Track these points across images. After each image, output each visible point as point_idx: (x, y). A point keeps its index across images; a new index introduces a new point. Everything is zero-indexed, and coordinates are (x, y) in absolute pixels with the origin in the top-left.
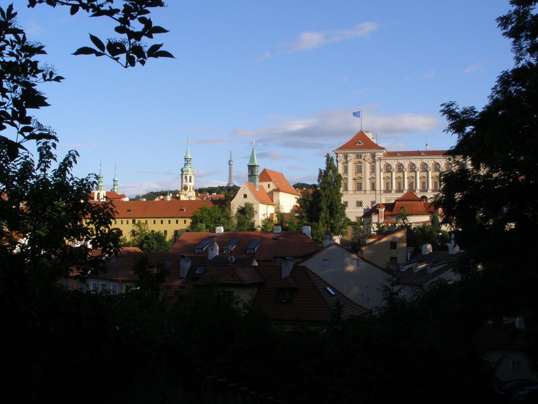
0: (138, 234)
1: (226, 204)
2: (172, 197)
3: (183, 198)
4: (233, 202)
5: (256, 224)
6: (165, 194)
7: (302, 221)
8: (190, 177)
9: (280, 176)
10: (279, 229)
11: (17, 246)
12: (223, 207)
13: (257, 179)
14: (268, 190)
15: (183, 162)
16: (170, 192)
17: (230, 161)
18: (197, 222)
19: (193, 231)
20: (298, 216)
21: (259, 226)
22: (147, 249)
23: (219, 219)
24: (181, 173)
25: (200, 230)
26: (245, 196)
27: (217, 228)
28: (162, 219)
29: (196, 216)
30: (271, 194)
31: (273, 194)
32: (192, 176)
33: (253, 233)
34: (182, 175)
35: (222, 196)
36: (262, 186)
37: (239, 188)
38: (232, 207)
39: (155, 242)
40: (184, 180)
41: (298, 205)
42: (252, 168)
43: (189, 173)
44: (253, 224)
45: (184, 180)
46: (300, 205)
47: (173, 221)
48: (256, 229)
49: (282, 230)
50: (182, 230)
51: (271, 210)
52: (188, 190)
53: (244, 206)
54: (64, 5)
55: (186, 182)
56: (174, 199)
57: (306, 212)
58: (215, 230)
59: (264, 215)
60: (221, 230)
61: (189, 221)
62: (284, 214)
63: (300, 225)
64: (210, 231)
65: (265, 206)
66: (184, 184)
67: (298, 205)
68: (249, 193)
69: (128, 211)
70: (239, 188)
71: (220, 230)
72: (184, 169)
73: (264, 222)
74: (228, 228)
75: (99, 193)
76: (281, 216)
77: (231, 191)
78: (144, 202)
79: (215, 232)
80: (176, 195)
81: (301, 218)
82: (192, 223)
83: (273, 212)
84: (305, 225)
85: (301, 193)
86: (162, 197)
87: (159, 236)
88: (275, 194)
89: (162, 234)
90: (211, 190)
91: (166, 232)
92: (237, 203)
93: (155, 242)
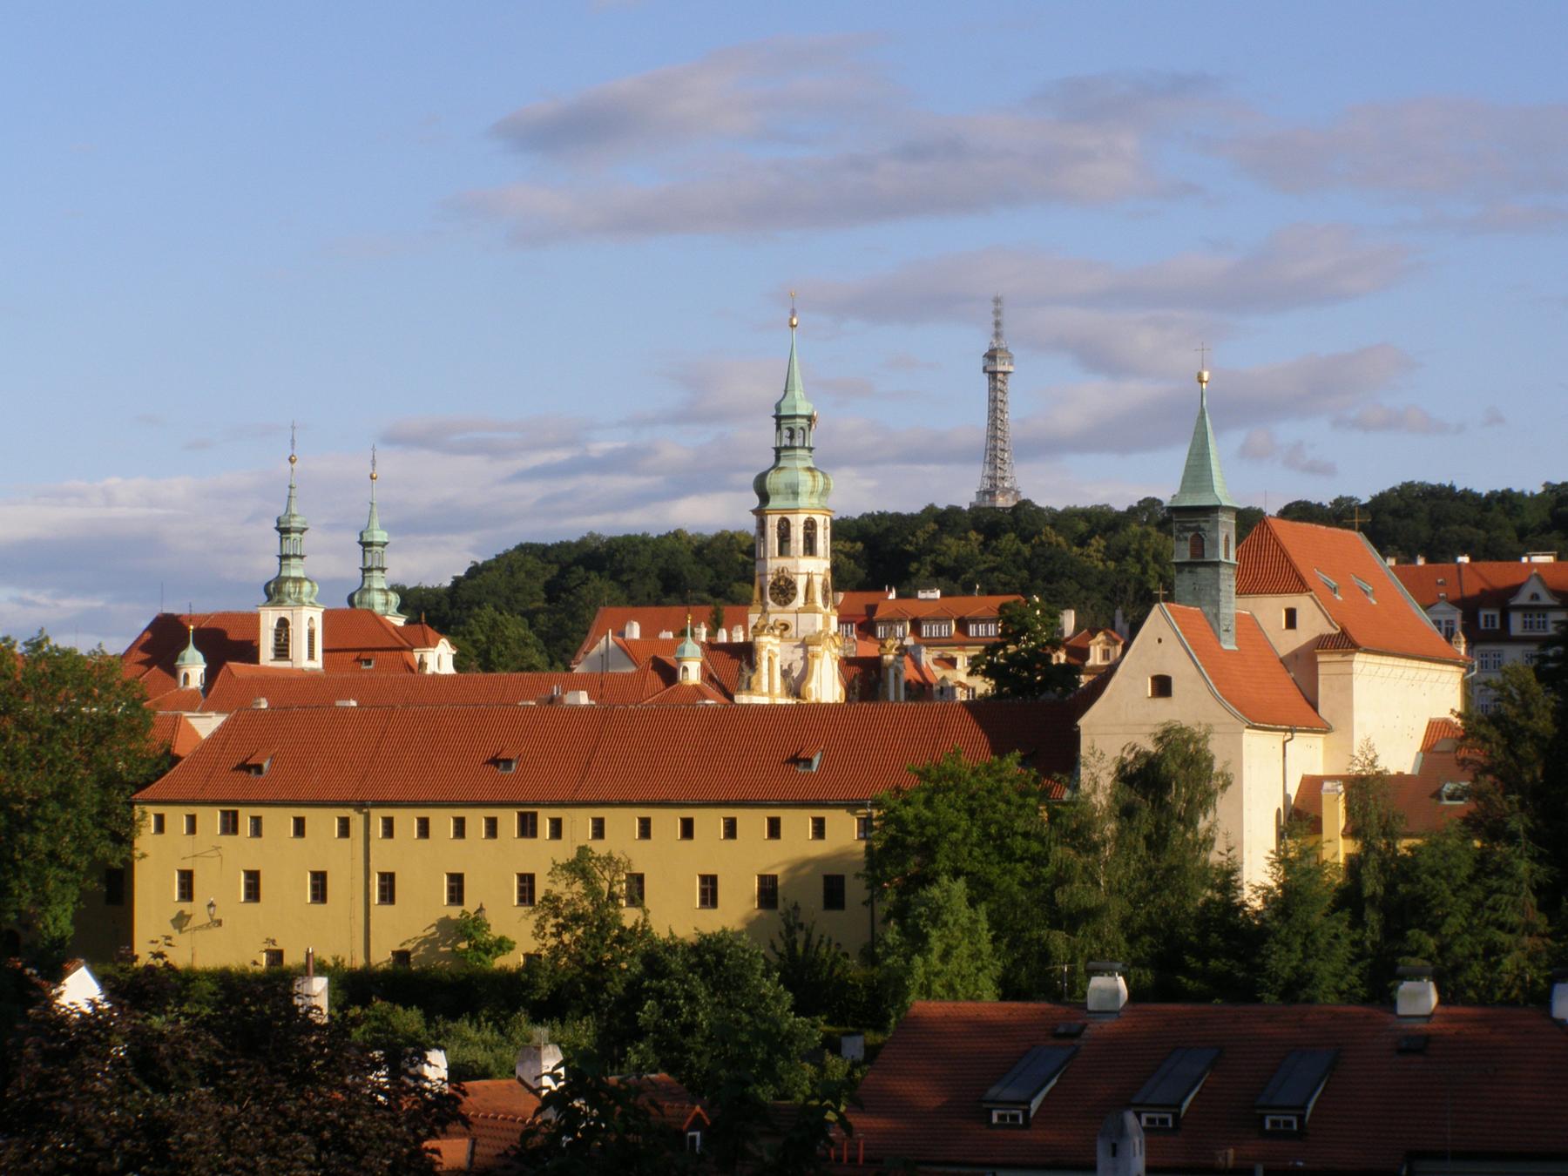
0: (576, 918)
4: (1088, 723)
8: (810, 526)
14: (1288, 643)
15: (768, 435)
17: (991, 356)
22: (658, 1029)
24: (755, 501)
26: (1162, 686)
30: (1303, 665)
36: (1252, 618)
39: (702, 992)
43: (803, 501)
47: (753, 821)
53: (1150, 747)
55: (783, 551)
65: (1273, 740)
69: (495, 761)
75: (283, 624)
78: (577, 709)
88: (1328, 665)
93: (702, 992)
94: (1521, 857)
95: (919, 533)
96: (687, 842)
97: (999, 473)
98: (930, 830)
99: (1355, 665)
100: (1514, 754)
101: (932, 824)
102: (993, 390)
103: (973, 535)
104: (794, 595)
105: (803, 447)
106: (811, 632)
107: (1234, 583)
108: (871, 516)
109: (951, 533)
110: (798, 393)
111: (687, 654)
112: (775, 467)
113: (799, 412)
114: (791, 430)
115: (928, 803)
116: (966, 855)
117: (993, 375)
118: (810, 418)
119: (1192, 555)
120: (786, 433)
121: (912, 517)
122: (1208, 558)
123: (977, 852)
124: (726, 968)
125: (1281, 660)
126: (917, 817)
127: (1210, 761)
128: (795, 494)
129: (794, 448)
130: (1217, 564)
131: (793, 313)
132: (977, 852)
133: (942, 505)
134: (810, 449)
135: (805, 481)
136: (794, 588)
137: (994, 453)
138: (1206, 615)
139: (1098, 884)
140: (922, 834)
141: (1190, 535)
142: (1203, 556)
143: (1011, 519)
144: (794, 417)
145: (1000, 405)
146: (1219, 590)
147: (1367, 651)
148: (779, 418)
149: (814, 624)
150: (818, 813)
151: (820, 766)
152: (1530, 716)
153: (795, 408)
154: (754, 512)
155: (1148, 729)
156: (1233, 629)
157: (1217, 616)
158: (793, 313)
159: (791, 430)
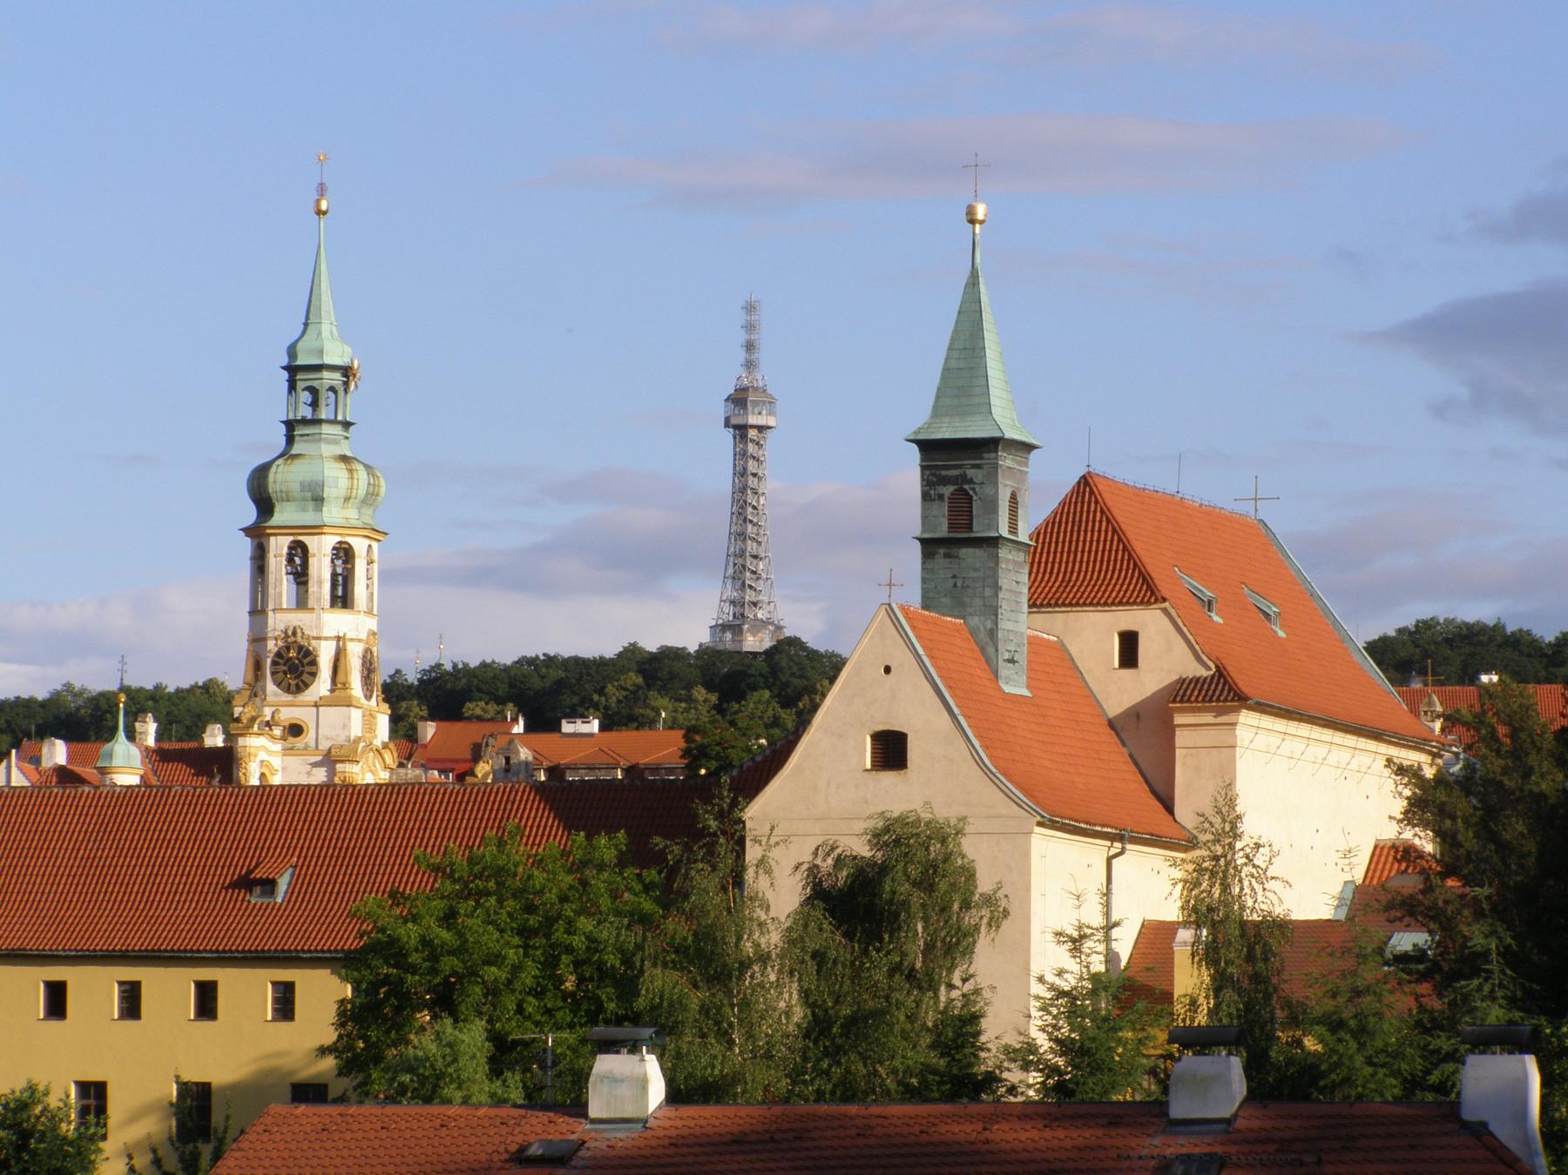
1: (692, 833)
2: (160, 756)
3: (266, 761)
4: (757, 813)
5: (996, 1031)
6: (86, 720)
7: (1463, 1004)
8: (344, 553)
9: (1241, 545)
10: (1220, 1088)
11: (1465, 930)
12: (659, 858)
13: (1015, 578)
14: (1122, 692)
16: (141, 702)
17: (739, 399)
18: (405, 1002)
19: (364, 1092)
20: (1419, 955)
21: (1025, 1055)
23: (627, 985)
24: (250, 514)
25: (428, 1086)
26: (891, 750)
27: (605, 1064)
28: (56, 973)
29: (390, 949)
30: (1148, 735)
31: (1168, 732)
32: (359, 545)
33: (954, 1124)
34: (257, 534)
35: (659, 747)
36: (1060, 647)
37: (832, 666)
38: (752, 853)
40: (281, 584)
41: (1426, 843)
42: (957, 466)
43: (332, 513)
44: (961, 1030)
45: (281, 584)
46: (1442, 835)
47: (170, 989)
48: (991, 1079)
49: (1256, 1094)
50: (254, 1092)
51: (1150, 888)
52: (322, 685)
54: (246, 545)
55: (302, 603)
56: (180, 773)
57: (1498, 911)
58: (580, 1079)
59: (1076, 943)
60: (643, 1083)
61: (323, 994)
62: (1282, 927)
63: (1443, 1043)
64: (534, 1099)
65: (1085, 855)
66: (277, 622)
67: (1426, 843)
68: (922, 717)
70: (832, 666)
71: (634, 1086)
72: (283, 478)
73: (1073, 1013)
74: (711, 1061)
76: (1246, 950)
77: (758, 695)
79: (578, 1108)
80: (195, 729)
81: (1443, 969)
82: (351, 1016)
83: (1171, 912)
84: (1486, 1042)
85: (1451, 721)
86: (57, 753)
87: (25, 1135)
88: (1192, 734)
89: (54, 1118)
90: (545, 691)
91: (94, 1095)
92: (808, 814)
94: (1492, 997)
95: (610, 689)
96: (55, 1024)
97: (749, 596)
98: (449, 964)
99: (1239, 731)
100: (1494, 838)
101: (451, 953)
102: (741, 455)
103: (700, 693)
104: (314, 675)
105: (334, 422)
106: (341, 740)
107: (1025, 578)
108: (531, 661)
109: (663, 690)
110: (327, 327)
111: (117, 761)
112: (286, 454)
113: (328, 360)
114: (314, 391)
115: (449, 918)
116: (512, 1007)
117: (741, 431)
118: (347, 371)
119: (952, 527)
120: (306, 397)
121: (601, 663)
122: (979, 531)
123: (531, 1005)
124: (34, 1154)
125: (1111, 724)
126: (425, 942)
127: (970, 874)
128: (319, 500)
129: (317, 422)
130: (995, 542)
131: (322, 190)
132: (531, 1005)
133: (651, 645)
134: (347, 425)
135: (336, 478)
136: (314, 663)
137: (741, 569)
138: (973, 633)
139: (731, 1042)
140: (434, 971)
141: (947, 490)
142: (970, 528)
143: (765, 669)
144: (319, 368)
145: (752, 482)
146: (997, 588)
147: (1262, 708)
148: (292, 370)
149: (346, 726)
150: (284, 975)
151: (290, 892)
152: (1527, 773)
153: (321, 352)
154: (248, 531)
155: (860, 826)
156: (1022, 657)
157: (993, 633)
158: (322, 190)
159: (314, 391)
